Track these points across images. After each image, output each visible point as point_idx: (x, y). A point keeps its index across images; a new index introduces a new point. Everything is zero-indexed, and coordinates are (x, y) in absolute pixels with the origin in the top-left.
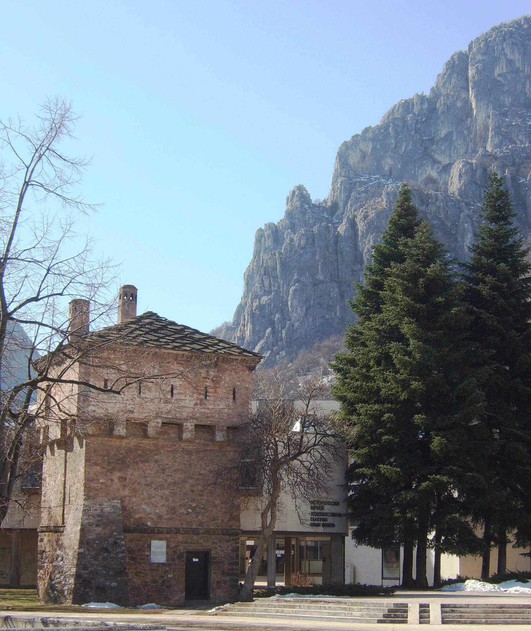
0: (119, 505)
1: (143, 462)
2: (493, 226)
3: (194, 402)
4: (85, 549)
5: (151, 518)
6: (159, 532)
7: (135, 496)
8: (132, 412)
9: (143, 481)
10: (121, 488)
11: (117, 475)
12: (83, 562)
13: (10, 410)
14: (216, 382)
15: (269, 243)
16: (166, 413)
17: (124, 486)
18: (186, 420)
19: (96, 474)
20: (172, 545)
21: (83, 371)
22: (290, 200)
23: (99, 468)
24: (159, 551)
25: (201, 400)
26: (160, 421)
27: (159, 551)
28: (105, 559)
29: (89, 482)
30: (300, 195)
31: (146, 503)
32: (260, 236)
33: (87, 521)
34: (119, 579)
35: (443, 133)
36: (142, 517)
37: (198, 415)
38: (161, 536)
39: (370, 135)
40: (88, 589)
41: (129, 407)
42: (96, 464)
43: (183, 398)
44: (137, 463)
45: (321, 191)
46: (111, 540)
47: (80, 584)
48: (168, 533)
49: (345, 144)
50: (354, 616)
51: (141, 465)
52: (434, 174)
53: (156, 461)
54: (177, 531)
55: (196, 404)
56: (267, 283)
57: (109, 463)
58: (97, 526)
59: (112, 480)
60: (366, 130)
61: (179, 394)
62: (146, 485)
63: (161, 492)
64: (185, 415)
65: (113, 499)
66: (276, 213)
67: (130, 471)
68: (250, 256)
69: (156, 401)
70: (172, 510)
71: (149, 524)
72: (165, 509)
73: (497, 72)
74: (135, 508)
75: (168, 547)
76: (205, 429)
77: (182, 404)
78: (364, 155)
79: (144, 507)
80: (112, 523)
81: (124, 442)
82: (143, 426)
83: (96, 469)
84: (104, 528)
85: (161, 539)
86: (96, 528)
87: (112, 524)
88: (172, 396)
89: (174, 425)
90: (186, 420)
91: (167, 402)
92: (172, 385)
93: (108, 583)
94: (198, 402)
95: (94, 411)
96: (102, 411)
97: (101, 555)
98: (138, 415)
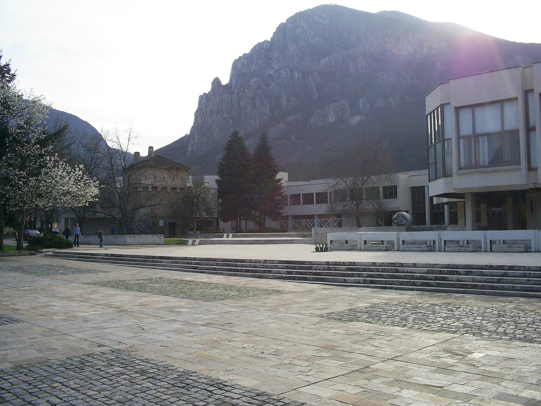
13: (82, 143)
14: (177, 175)
15: (204, 101)
22: (213, 83)
24: (161, 223)
27: (161, 223)
30: (216, 82)
32: (201, 98)
35: (276, 56)
39: (246, 57)
40: (314, 215)
45: (225, 80)
49: (236, 60)
50: (449, 281)
52: (272, 73)
54: (166, 217)
56: (203, 118)
60: (244, 55)
66: (208, 89)
68: (197, 107)
73: (298, 31)
76: (174, 189)
78: (243, 64)
81: (151, 193)
89: (165, 188)
98: (155, 185)
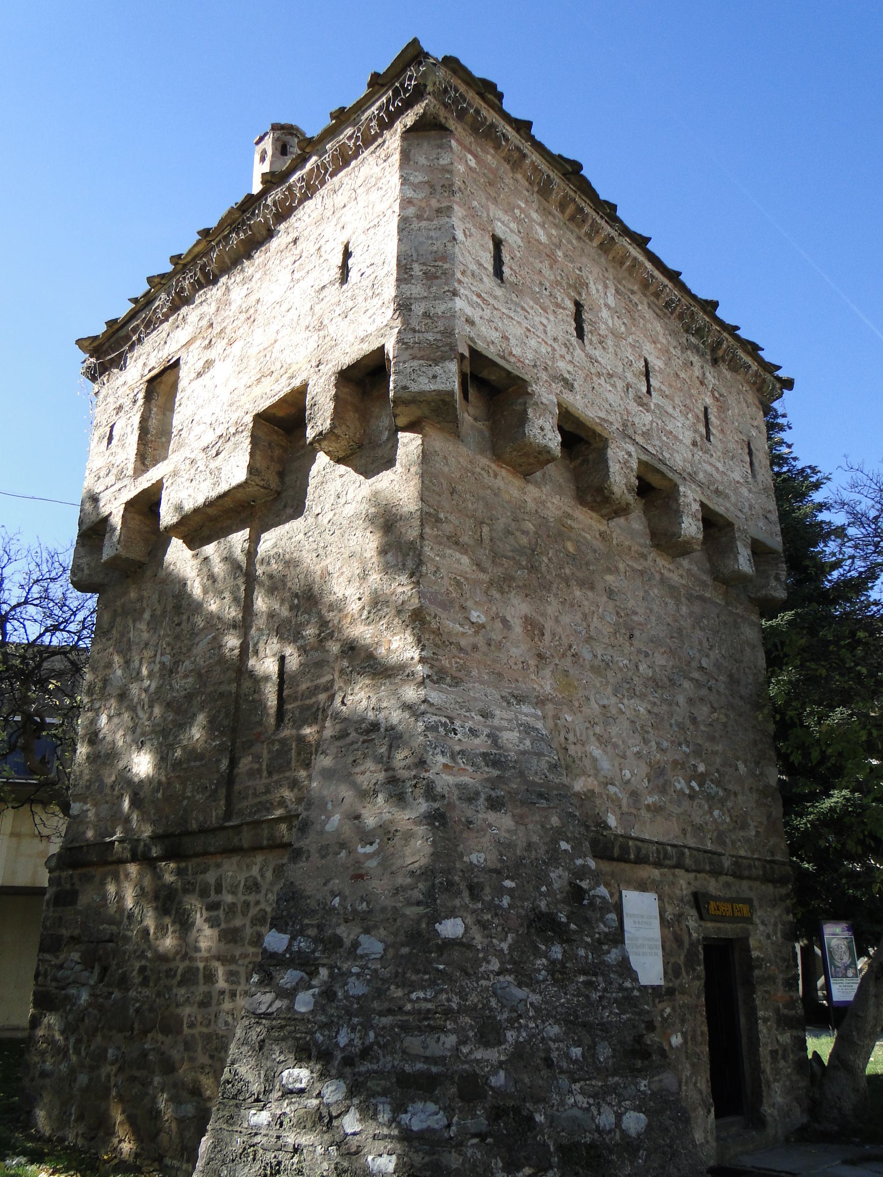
1: (582, 584)
2: (121, 765)
4: (469, 920)
6: (641, 860)
10: (532, 662)
12: (473, 998)
17: (540, 656)
19: (458, 584)
21: (418, 177)
23: (465, 560)
28: (559, 973)
29: (439, 611)
33: (450, 779)
34: (643, 1084)
36: (592, 792)
46: (559, 877)
47: (482, 1136)
48: (658, 864)
53: (610, 593)
57: (496, 557)
58: (495, 804)
74: (572, 749)
80: (541, 795)
83: (458, 561)
84: (520, 820)
86: (491, 817)
87: (543, 803)
93: (606, 1119)
96: (495, 336)
97: (538, 954)
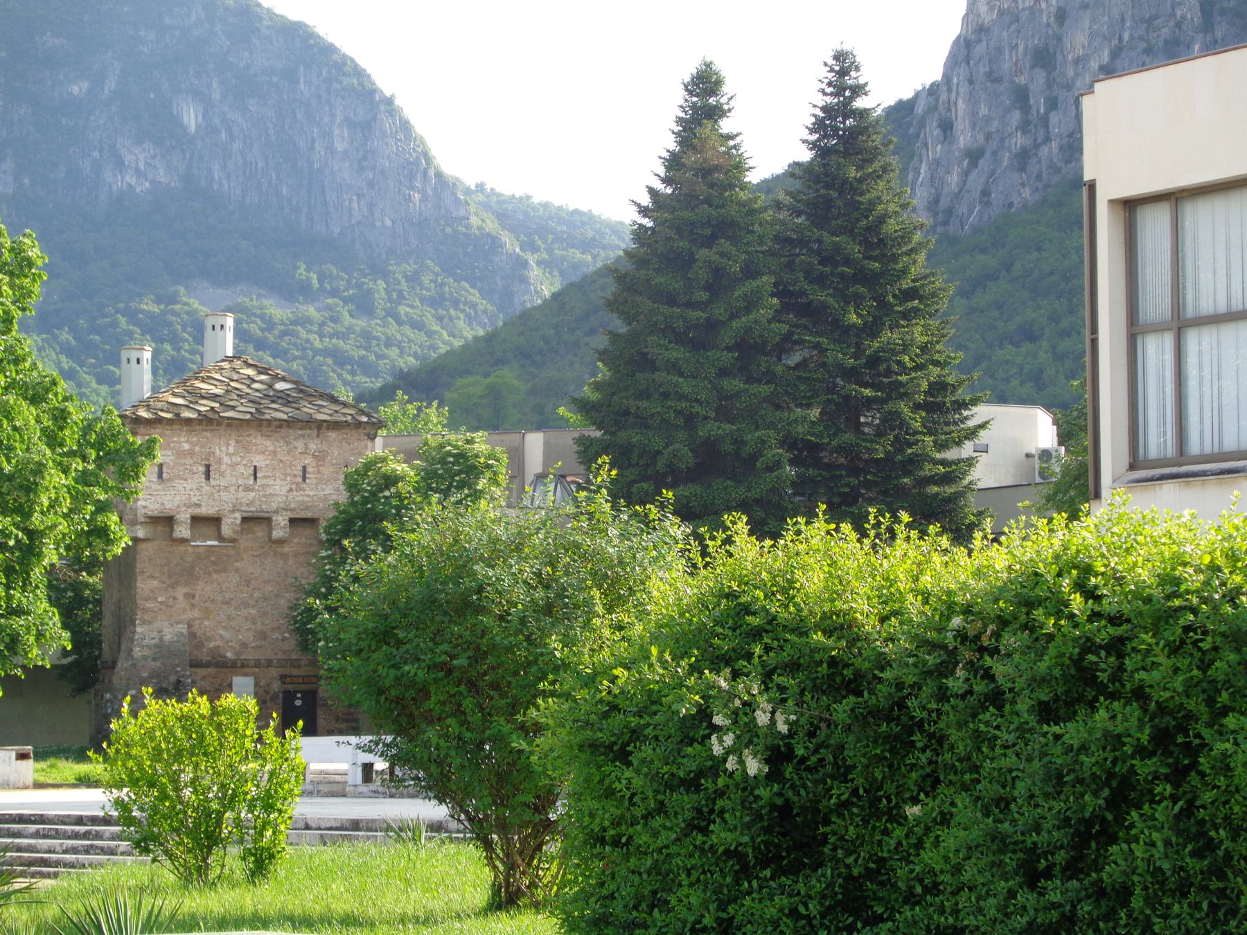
0: (184, 631)
1: (217, 572)
3: (288, 488)
5: (232, 647)
6: (243, 666)
7: (208, 618)
8: (198, 505)
9: (219, 598)
11: (181, 591)
16: (247, 505)
18: (276, 512)
20: (263, 683)
25: (298, 484)
26: (238, 516)
31: (224, 628)
37: (293, 505)
38: (246, 670)
41: (195, 500)
42: (152, 577)
43: (272, 482)
44: (209, 573)
48: (256, 667)
51: (215, 576)
53: (237, 570)
55: (291, 490)
59: (175, 598)
61: (265, 477)
62: (223, 603)
63: (244, 612)
64: (274, 506)
65: (177, 623)
67: (201, 585)
69: (232, 489)
70: (262, 635)
71: (229, 655)
72: (251, 634)
75: (256, 685)
77: (269, 491)
79: (221, 632)
82: (216, 521)
85: (246, 675)
88: (255, 478)
90: (276, 512)
91: (248, 489)
92: (255, 467)
94: (294, 486)
95: (145, 507)
96: (157, 506)
